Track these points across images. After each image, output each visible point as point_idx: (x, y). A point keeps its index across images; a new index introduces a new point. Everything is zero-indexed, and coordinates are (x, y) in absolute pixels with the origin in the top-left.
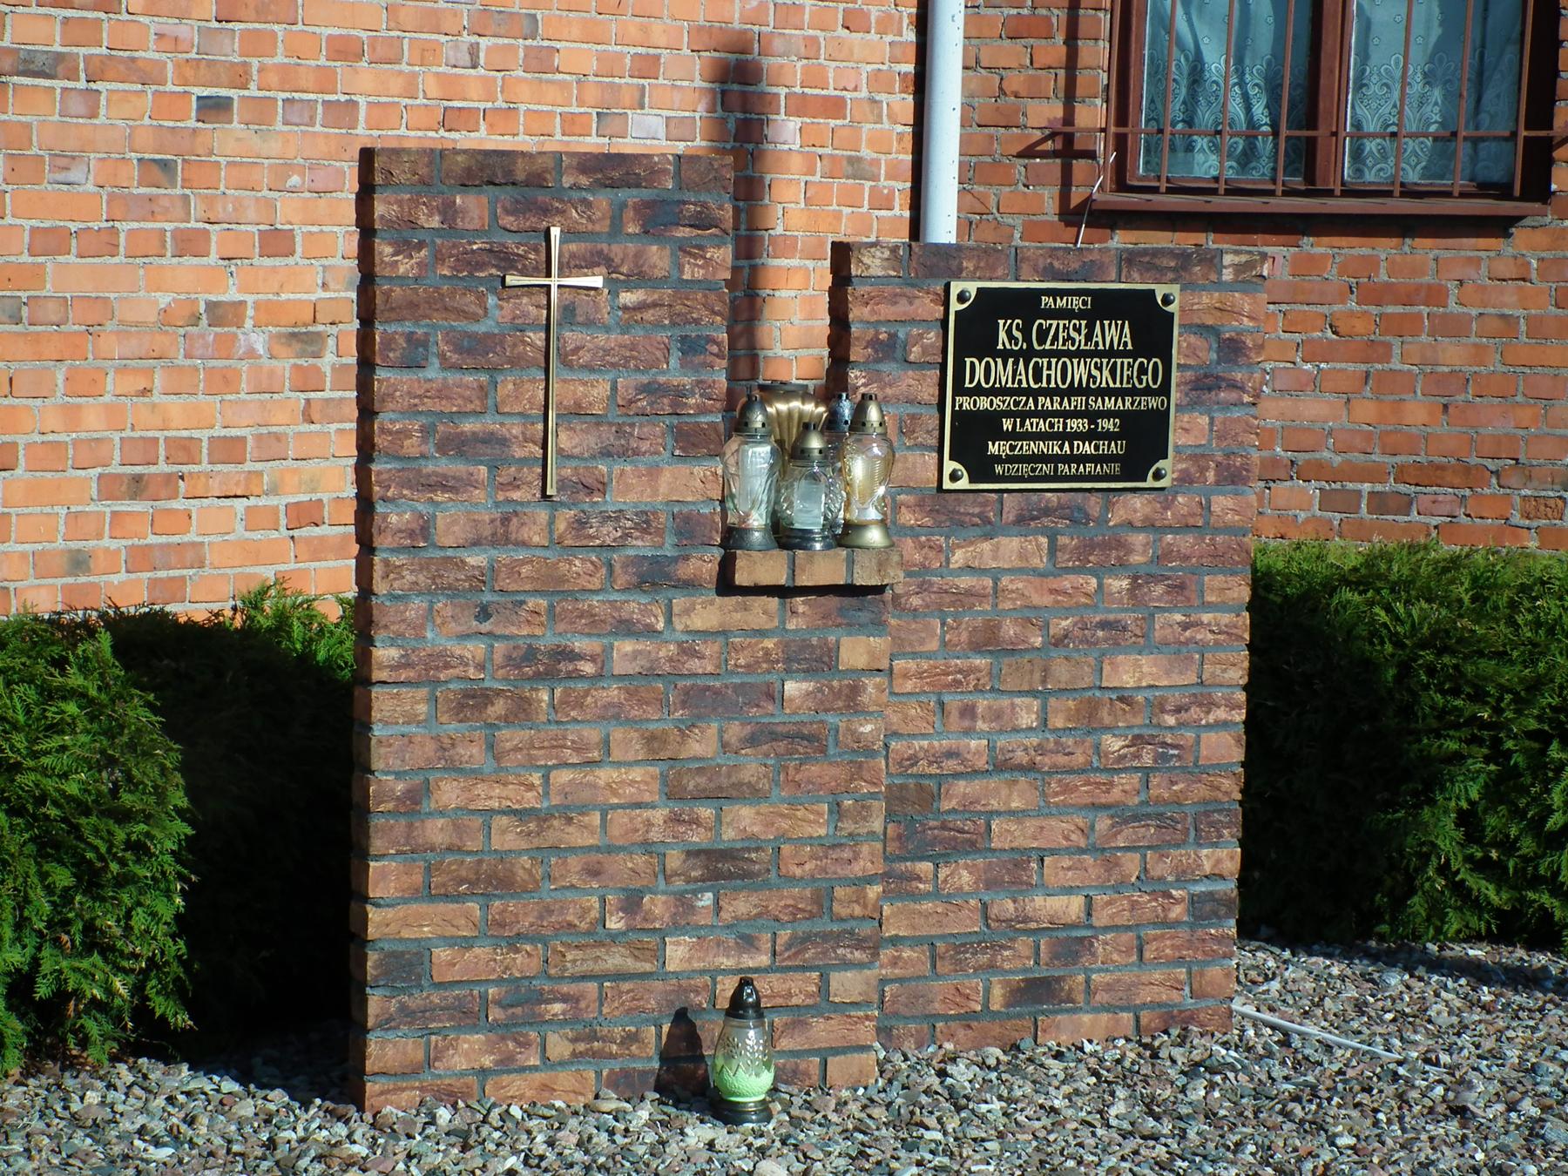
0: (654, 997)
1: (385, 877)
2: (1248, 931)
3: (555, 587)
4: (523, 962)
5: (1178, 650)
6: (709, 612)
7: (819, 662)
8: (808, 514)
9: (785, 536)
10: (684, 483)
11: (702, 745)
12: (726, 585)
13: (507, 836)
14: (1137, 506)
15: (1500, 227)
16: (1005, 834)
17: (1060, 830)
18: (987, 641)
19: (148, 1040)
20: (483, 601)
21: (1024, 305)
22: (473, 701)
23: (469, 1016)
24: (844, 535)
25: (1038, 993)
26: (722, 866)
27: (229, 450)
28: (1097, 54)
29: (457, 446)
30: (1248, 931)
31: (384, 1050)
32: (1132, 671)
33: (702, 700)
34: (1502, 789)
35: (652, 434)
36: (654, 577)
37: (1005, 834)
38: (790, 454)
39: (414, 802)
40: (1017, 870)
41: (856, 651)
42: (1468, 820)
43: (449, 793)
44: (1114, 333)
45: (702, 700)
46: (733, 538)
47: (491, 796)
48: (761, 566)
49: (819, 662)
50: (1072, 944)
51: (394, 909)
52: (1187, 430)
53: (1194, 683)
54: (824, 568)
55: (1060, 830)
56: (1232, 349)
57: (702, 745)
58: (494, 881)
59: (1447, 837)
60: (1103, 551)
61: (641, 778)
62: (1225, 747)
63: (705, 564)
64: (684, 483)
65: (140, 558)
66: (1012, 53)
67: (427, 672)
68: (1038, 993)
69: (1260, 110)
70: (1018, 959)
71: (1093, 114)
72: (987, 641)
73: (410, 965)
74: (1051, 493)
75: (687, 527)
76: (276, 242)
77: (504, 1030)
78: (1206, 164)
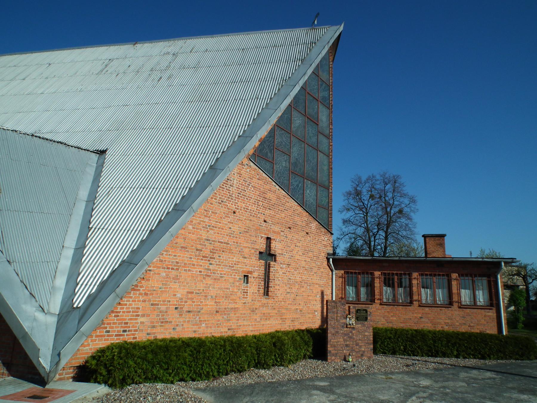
0: (343, 355)
1: (329, 346)
2: (375, 351)
3: (338, 328)
4: (336, 352)
5: (369, 332)
6: (346, 329)
7: (351, 332)
8: (351, 323)
9: (350, 324)
10: (344, 321)
11: (345, 338)
12: (347, 327)
13: (335, 343)
14: (366, 323)
15: (372, 304)
16: (360, 344)
17: (363, 344)
18: (358, 331)
19: (310, 358)
20: (334, 328)
21: (360, 310)
22: (333, 334)
23: (333, 355)
24: (353, 324)
25: (362, 355)
26: (347, 345)
27: (297, 318)
28: (343, 292)
29: (332, 318)
30: (375, 351)
31: (329, 357)
32: (366, 334)
33: (345, 335)
34: (382, 343)
35: (342, 318)
36: (343, 327)
37: (360, 344)
38: (350, 319)
39: (330, 341)
40: (361, 347)
41: (353, 332)
42: (380, 345)
43: (332, 340)
44: (364, 312)
45: (345, 335)
46: (347, 324)
47: (335, 341)
48: (349, 326)
49: (351, 332)
50: (364, 352)
51: (330, 348)
52: (369, 318)
53: (369, 334)
54: (352, 326)
55: (363, 344)
56: (371, 313)
57: (345, 338)
58: (335, 346)
59: (379, 346)
60: (364, 325)
61: (342, 340)
62: (372, 339)
63: (345, 326)
64: (344, 321)
65: (293, 326)
66: (338, 292)
67: (331, 332)
68: (362, 355)
69: (526, 331)
70: (361, 353)
71: (343, 296)
72: (358, 331)
73: (330, 351)
74: (361, 322)
75: (344, 323)
76: (300, 304)
77: (335, 356)
78: (351, 299)
